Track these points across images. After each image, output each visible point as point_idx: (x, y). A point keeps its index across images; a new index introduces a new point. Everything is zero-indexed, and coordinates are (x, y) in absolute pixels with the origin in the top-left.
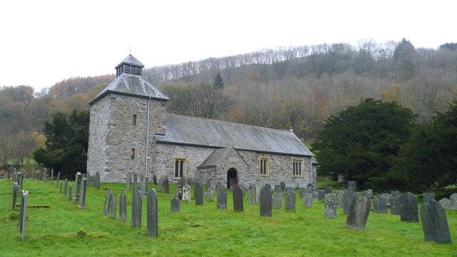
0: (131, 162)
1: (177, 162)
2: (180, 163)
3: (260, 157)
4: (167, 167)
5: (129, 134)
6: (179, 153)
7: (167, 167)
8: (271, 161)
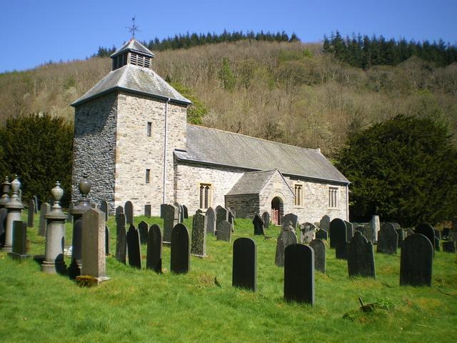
0: (147, 188)
1: (202, 188)
2: (205, 187)
3: (295, 182)
4: (190, 195)
5: (143, 148)
6: (205, 175)
7: (190, 195)
8: (306, 188)
